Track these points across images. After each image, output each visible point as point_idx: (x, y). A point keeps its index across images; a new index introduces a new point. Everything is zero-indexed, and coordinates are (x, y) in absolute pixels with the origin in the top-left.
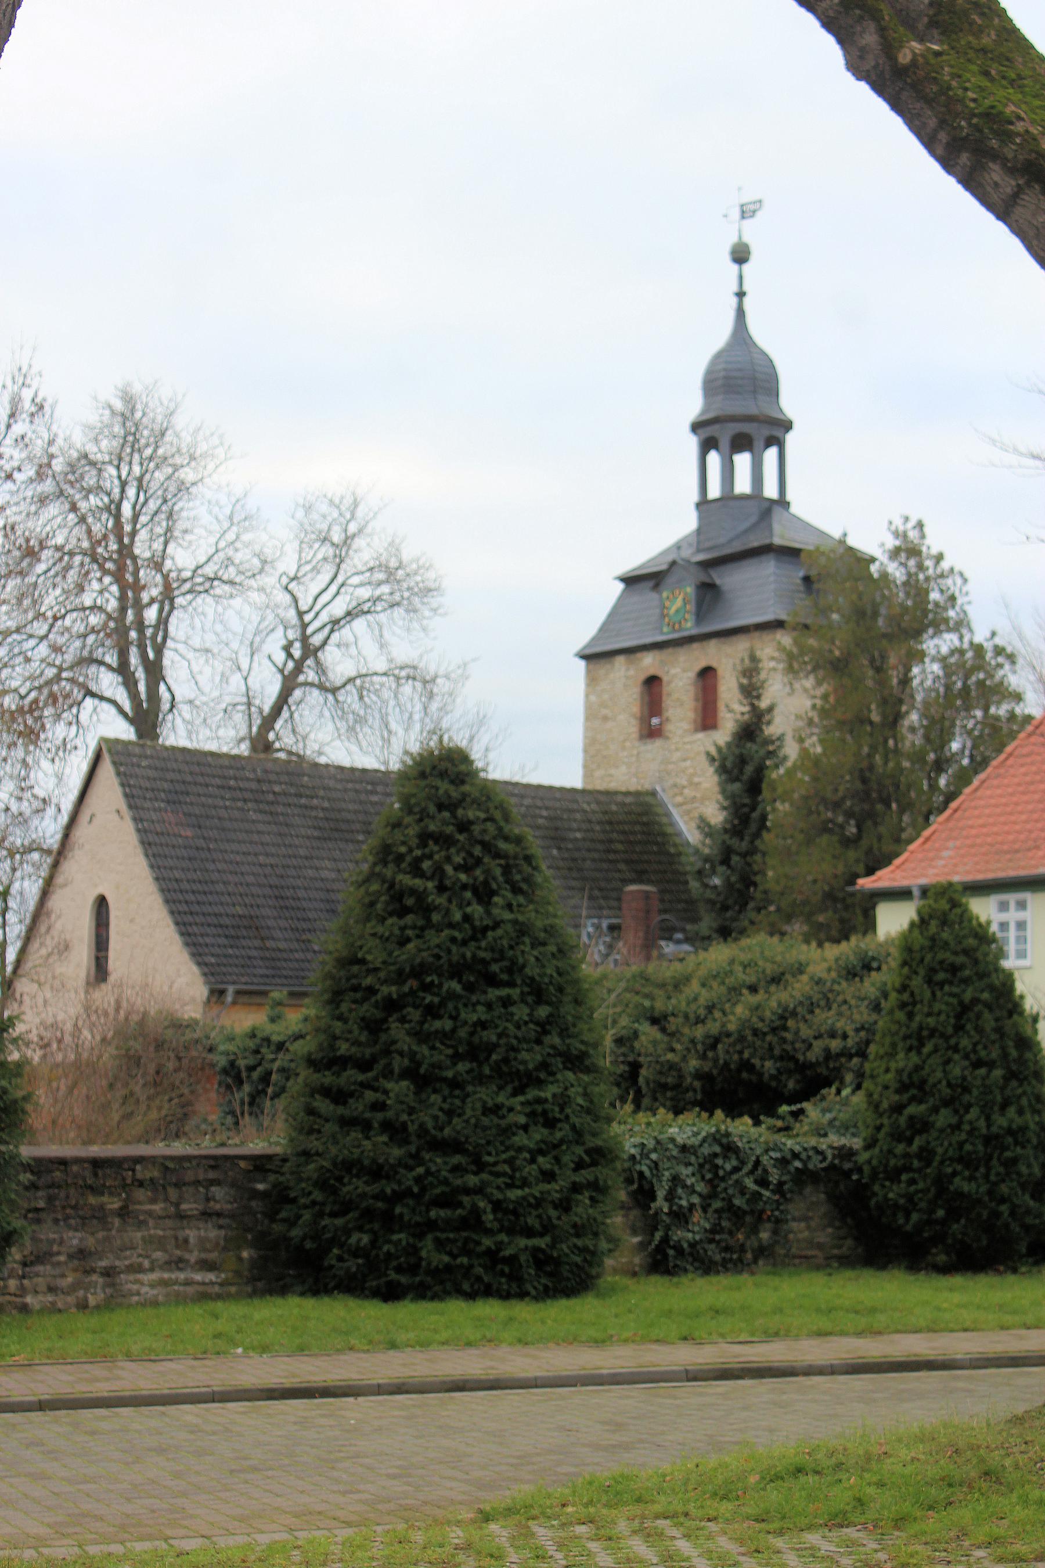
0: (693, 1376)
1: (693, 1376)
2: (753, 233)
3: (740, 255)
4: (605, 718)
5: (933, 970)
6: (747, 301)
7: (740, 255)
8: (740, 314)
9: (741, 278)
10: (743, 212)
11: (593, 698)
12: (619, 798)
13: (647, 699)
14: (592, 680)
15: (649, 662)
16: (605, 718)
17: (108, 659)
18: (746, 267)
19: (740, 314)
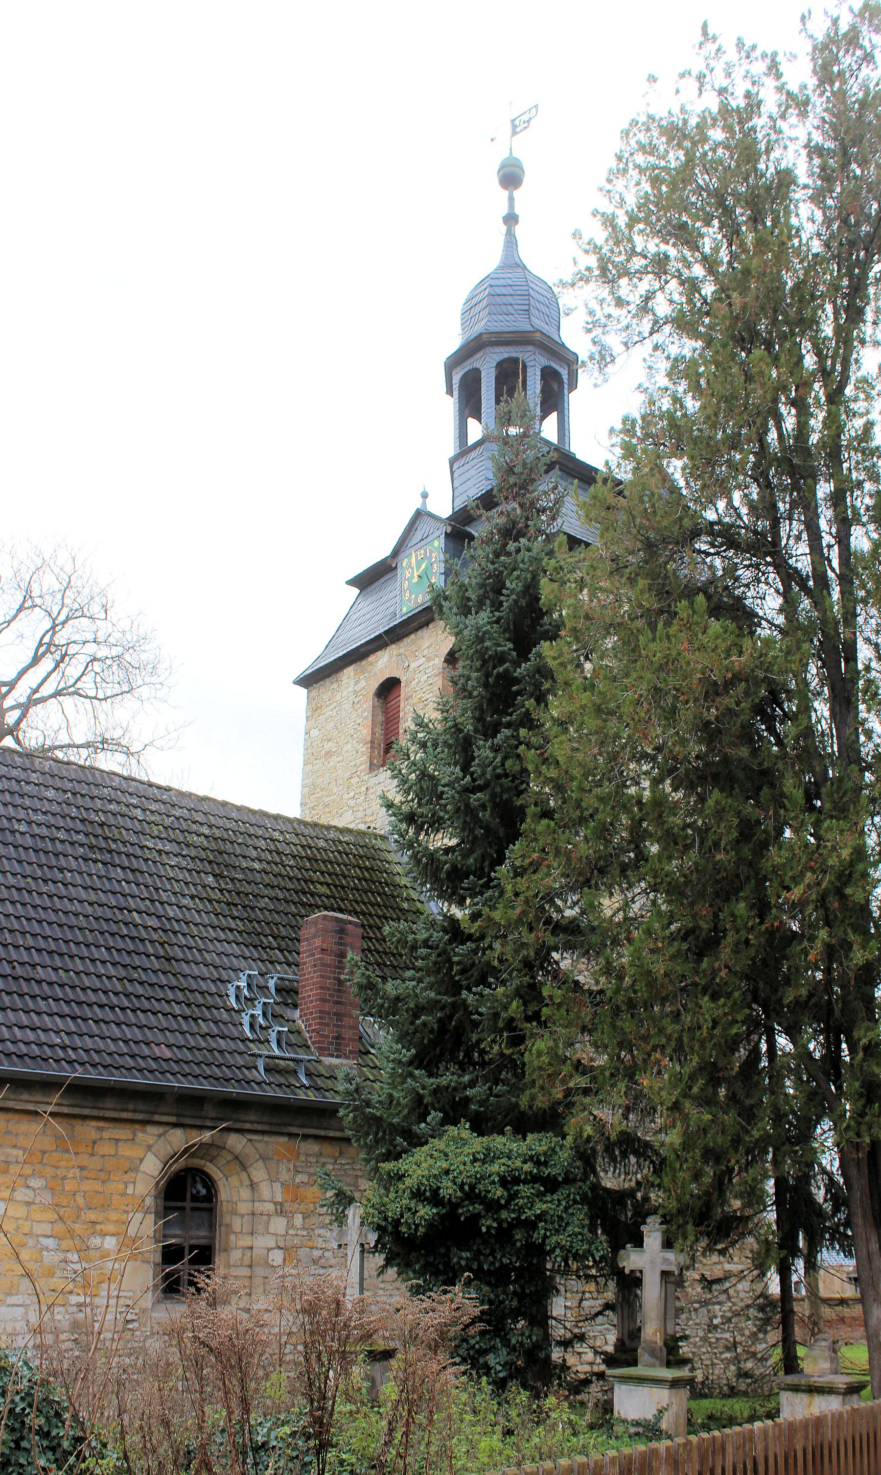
0: (876, 1452)
1: (876, 1452)
2: (525, 150)
3: (511, 178)
4: (329, 754)
5: (640, 528)
6: (518, 230)
7: (511, 178)
8: (511, 242)
9: (511, 219)
10: (514, 127)
11: (315, 733)
12: (332, 835)
13: (380, 718)
14: (314, 710)
15: (383, 665)
16: (329, 754)
17: (249, 1255)
18: (516, 193)
19: (511, 242)
